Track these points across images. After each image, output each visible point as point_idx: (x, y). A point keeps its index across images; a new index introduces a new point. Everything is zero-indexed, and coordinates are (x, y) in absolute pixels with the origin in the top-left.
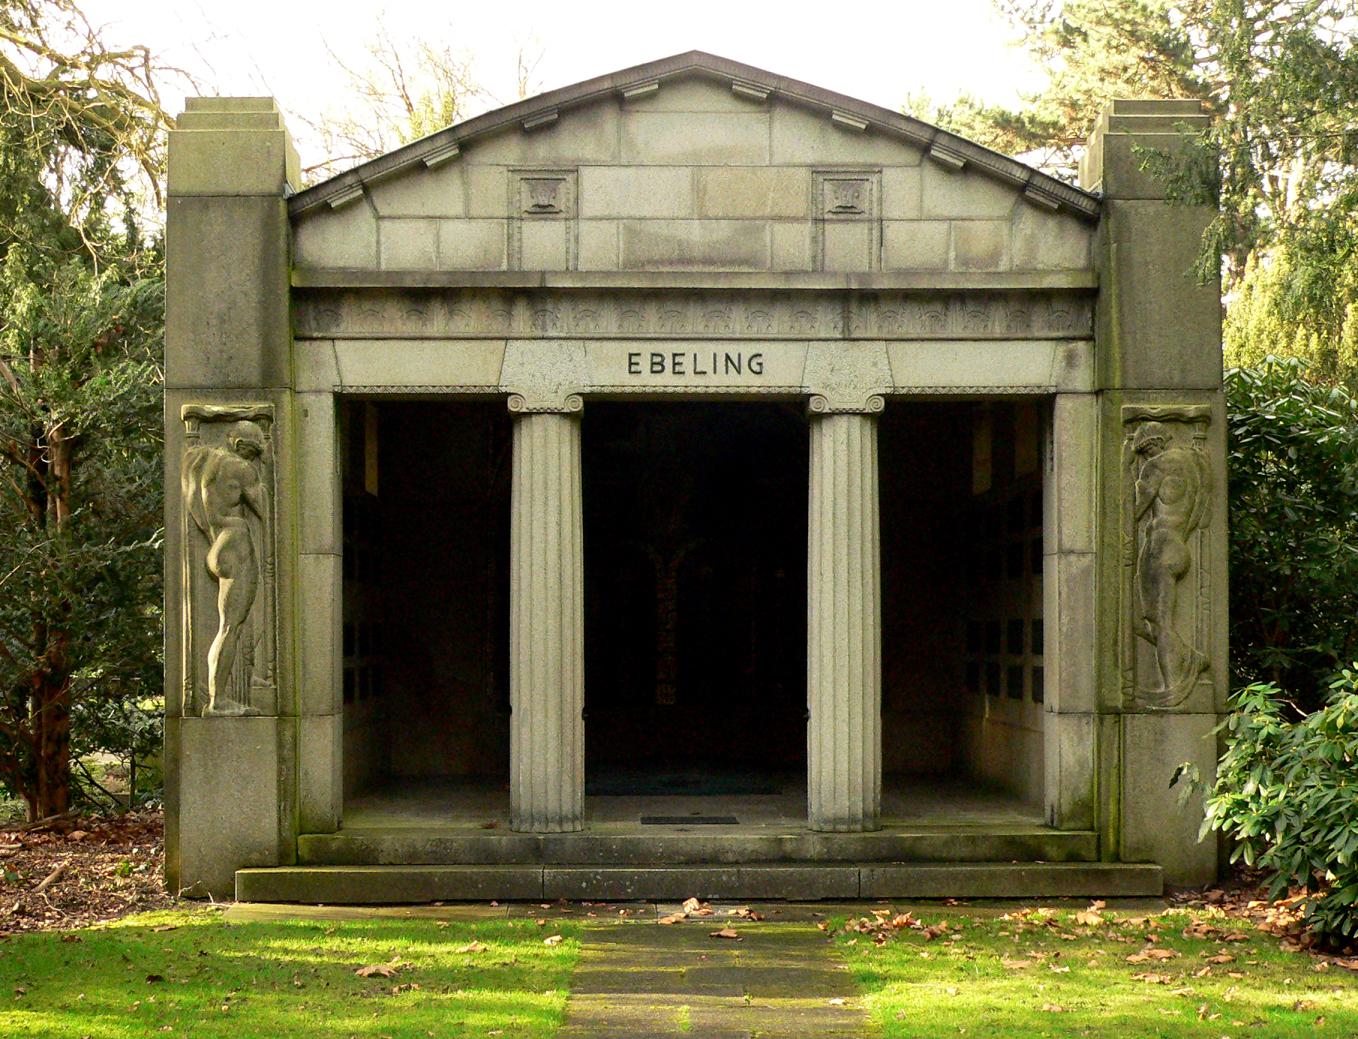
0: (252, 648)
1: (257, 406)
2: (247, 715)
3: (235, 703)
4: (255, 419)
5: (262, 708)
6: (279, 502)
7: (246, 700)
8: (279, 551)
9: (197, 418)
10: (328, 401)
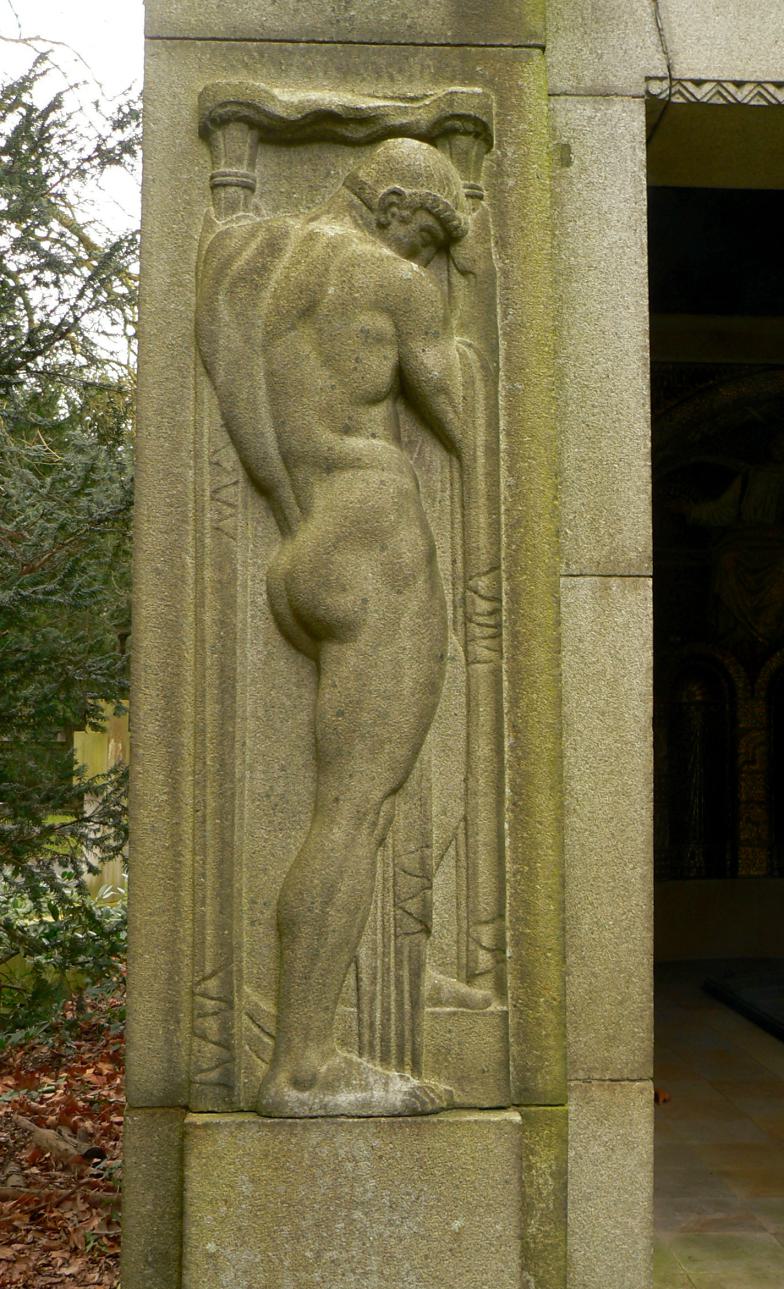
0: (426, 876)
1: (428, 93)
2: (416, 1112)
3: (370, 1066)
4: (437, 133)
5: (461, 1080)
6: (511, 394)
7: (406, 1054)
8: (514, 560)
9: (251, 124)
10: (632, 122)
